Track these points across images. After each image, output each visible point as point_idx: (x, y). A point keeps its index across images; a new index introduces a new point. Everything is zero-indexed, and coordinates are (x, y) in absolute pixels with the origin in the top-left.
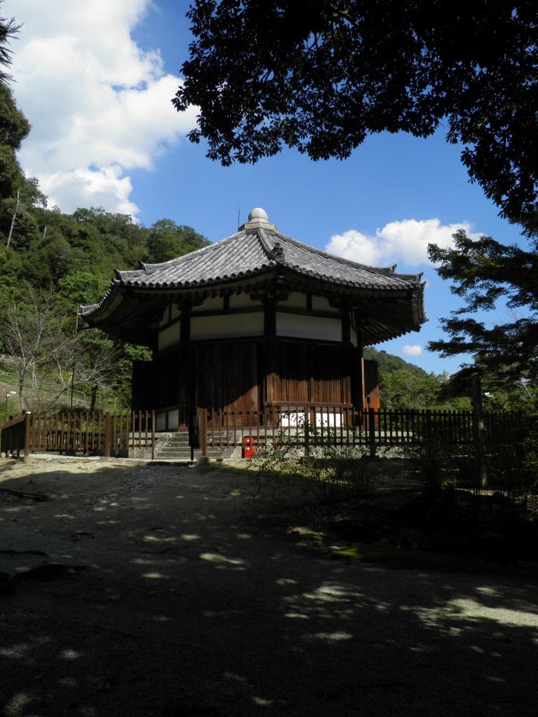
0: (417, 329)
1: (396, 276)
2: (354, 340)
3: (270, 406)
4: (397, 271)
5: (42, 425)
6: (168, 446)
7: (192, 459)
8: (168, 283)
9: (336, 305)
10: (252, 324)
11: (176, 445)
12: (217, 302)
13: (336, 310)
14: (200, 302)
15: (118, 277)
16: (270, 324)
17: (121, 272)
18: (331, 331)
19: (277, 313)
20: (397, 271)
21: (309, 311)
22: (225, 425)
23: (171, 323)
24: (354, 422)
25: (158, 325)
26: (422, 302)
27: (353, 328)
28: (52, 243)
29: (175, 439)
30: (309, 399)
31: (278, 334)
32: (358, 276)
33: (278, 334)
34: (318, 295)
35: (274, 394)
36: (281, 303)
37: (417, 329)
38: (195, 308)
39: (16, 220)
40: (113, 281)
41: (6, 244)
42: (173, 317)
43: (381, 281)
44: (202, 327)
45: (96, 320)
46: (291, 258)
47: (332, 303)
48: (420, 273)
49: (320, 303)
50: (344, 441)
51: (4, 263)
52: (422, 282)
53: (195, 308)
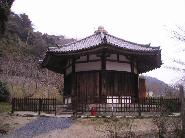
0: (159, 67)
1: (150, 47)
2: (135, 72)
3: (103, 95)
4: (151, 46)
5: (46, 102)
6: (65, 110)
7: (55, 116)
8: (66, 51)
9: (128, 59)
10: (97, 66)
11: (68, 110)
12: (84, 58)
13: (128, 61)
14: (79, 58)
15: (49, 49)
16: (103, 66)
17: (50, 48)
18: (127, 69)
19: (106, 62)
20: (151, 46)
21: (118, 61)
22: (87, 102)
23: (69, 66)
24: (134, 102)
25: (66, 66)
26: (160, 57)
27: (135, 67)
28: (40, 42)
29: (68, 108)
30: (118, 93)
31: (106, 69)
32: (136, 48)
33: (106, 69)
34: (121, 55)
35: (105, 91)
36: (107, 58)
37: (159, 67)
38: (77, 61)
39: (29, 35)
40: (47, 51)
41: (26, 43)
42: (70, 64)
43: (143, 49)
44: (79, 68)
45: (44, 65)
46: (110, 41)
47: (127, 58)
48: (159, 46)
49: (122, 58)
50: (123, 110)
51: (25, 49)
52: (160, 49)
53: (77, 61)
